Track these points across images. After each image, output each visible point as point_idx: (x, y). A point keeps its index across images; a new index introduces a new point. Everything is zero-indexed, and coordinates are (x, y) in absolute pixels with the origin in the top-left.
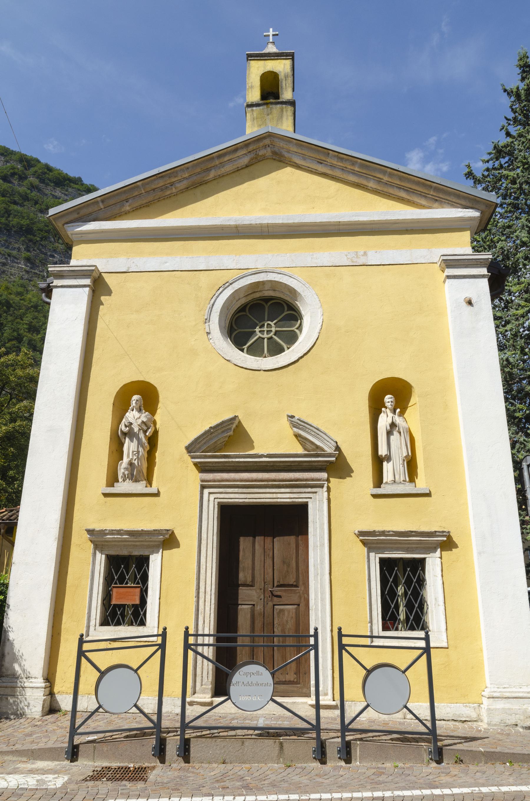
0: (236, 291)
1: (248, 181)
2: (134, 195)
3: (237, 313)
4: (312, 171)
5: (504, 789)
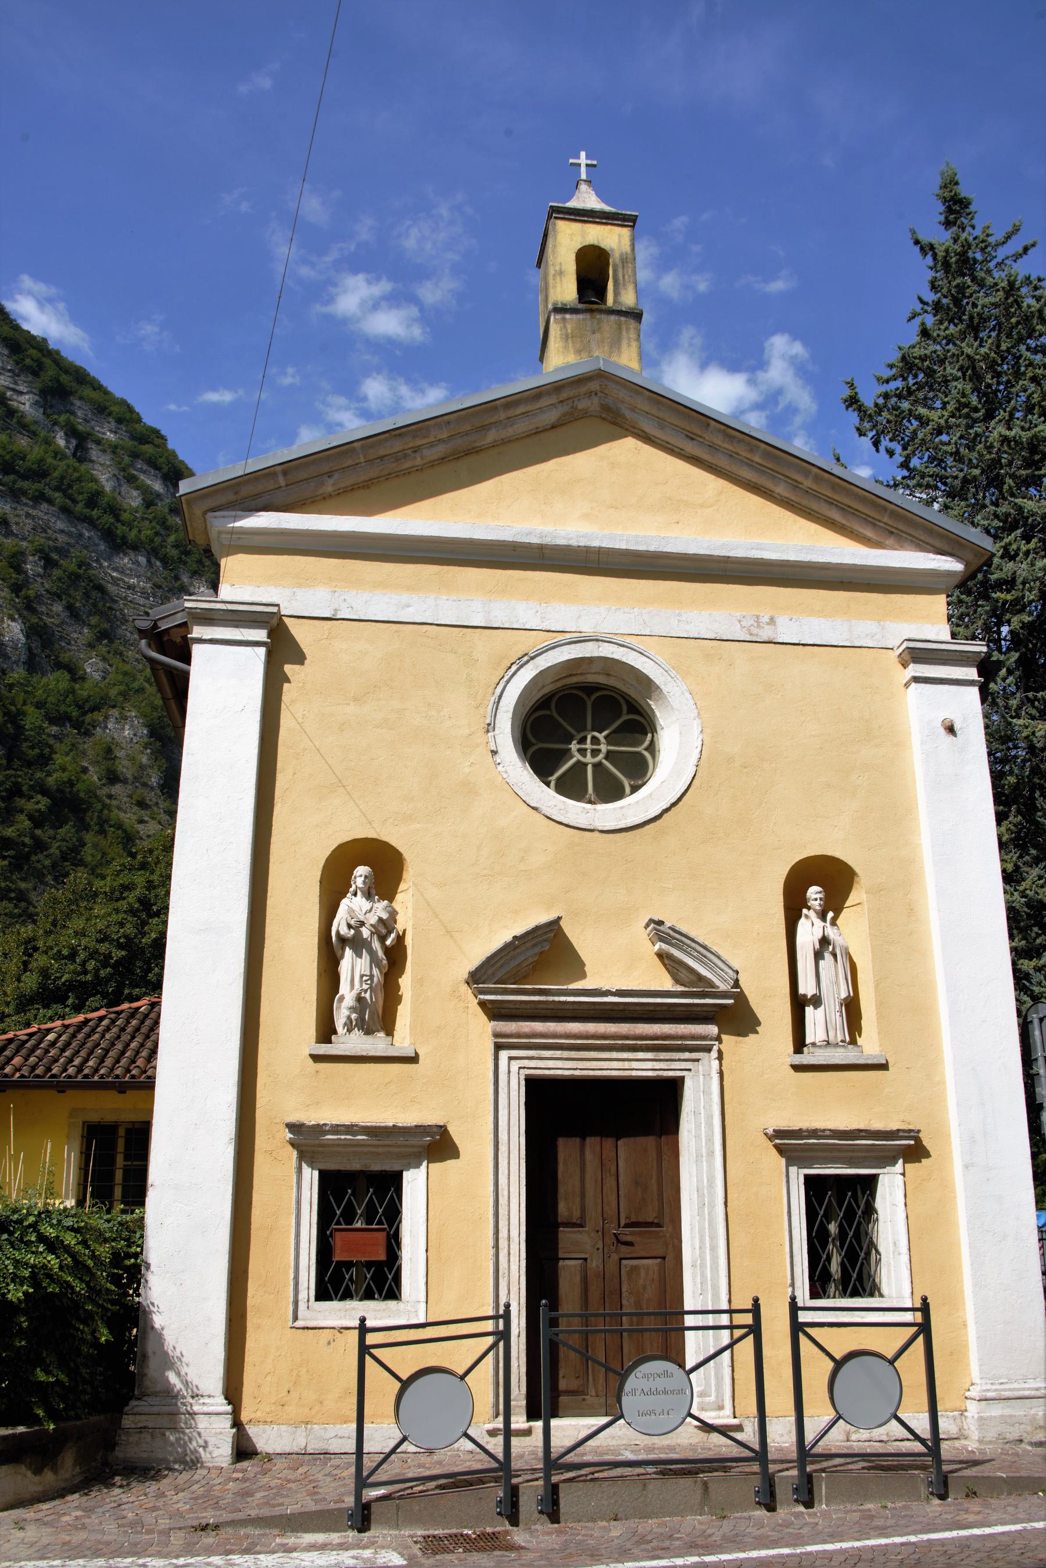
0: (541, 672)
1: (556, 457)
2: (343, 466)
4: (673, 451)
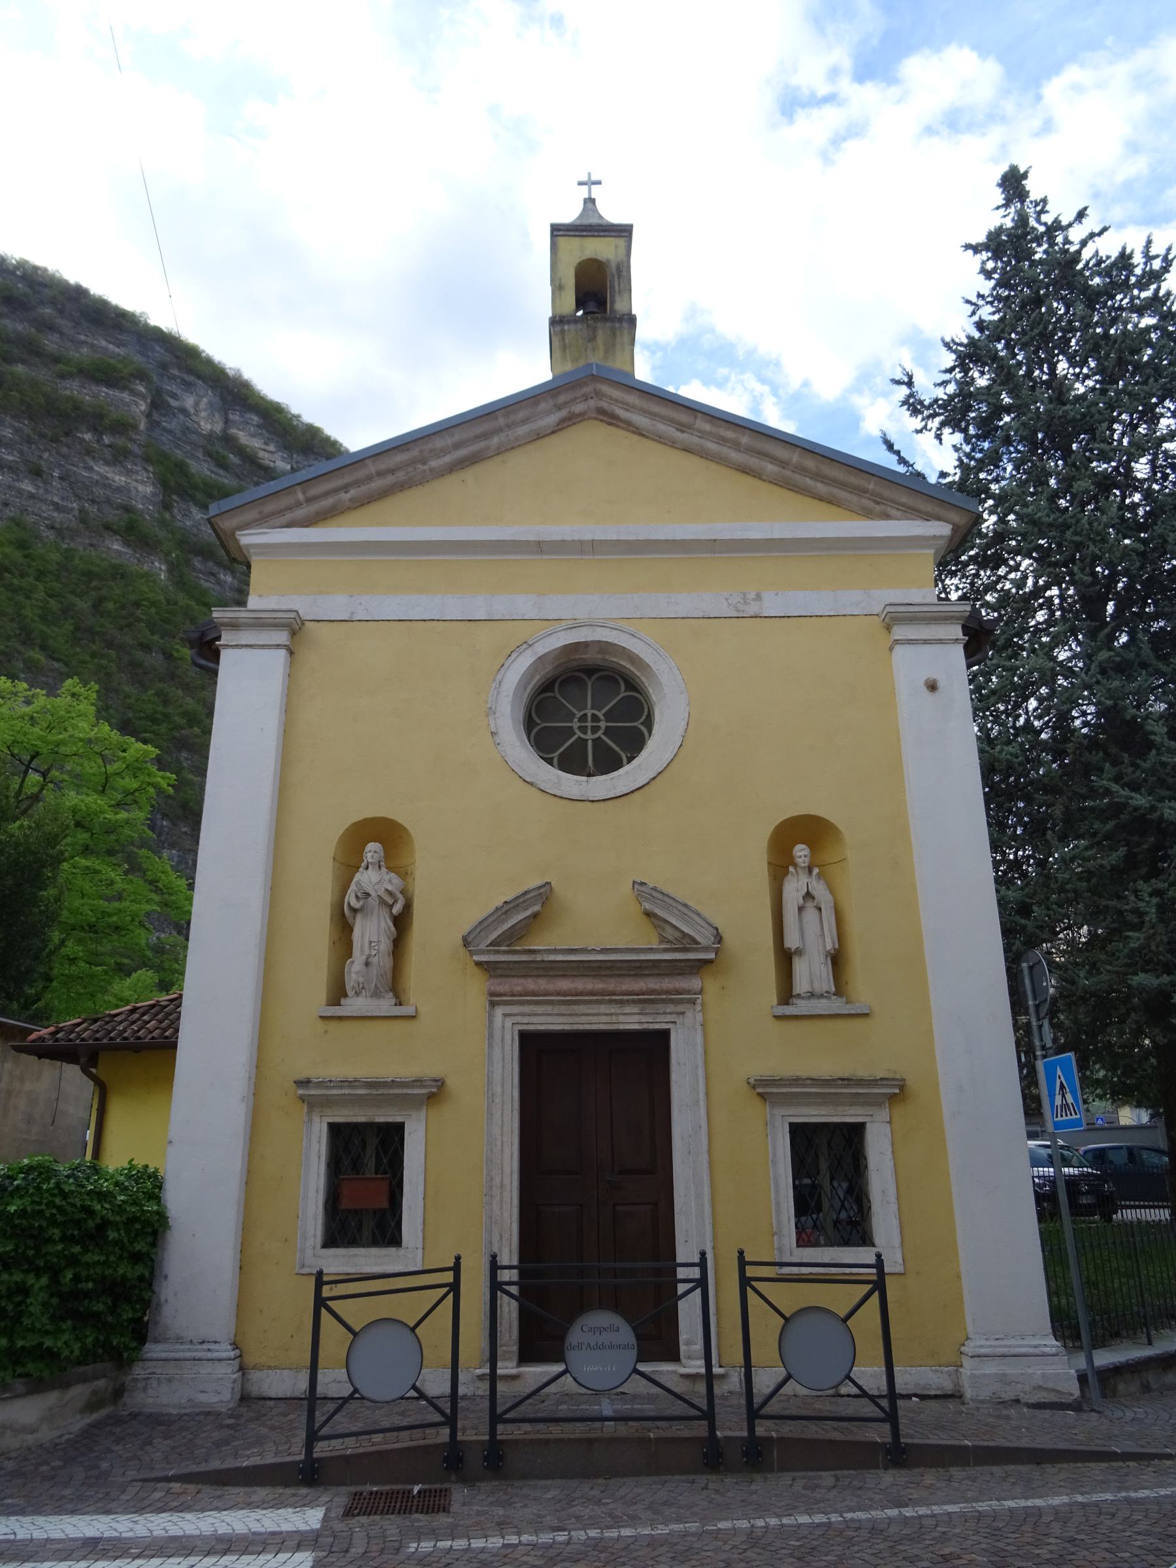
0: (540, 658)
3: (539, 694)
5: (1010, 1504)
